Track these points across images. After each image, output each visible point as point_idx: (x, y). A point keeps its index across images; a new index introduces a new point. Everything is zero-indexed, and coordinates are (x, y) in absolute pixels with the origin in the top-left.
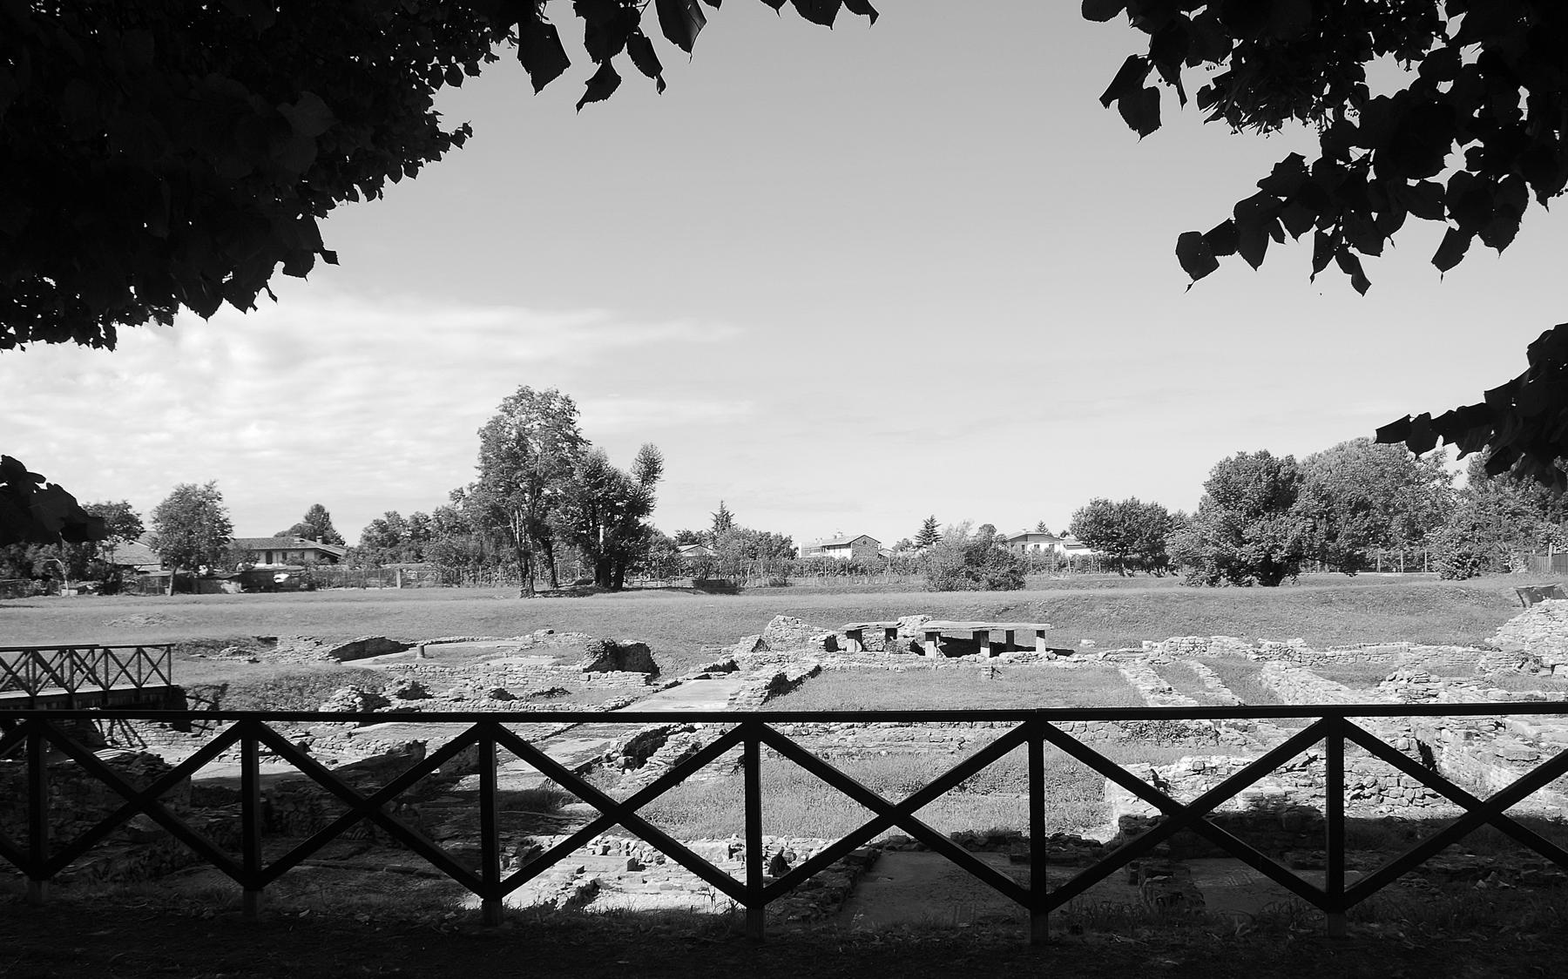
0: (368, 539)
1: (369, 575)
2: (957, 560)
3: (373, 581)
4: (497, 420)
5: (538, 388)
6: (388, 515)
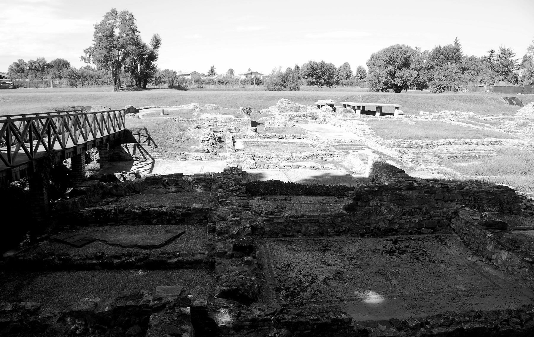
0: (12, 70)
1: (39, 83)
2: (279, 80)
3: (41, 85)
4: (104, 21)
5: (120, 10)
6: (19, 61)
